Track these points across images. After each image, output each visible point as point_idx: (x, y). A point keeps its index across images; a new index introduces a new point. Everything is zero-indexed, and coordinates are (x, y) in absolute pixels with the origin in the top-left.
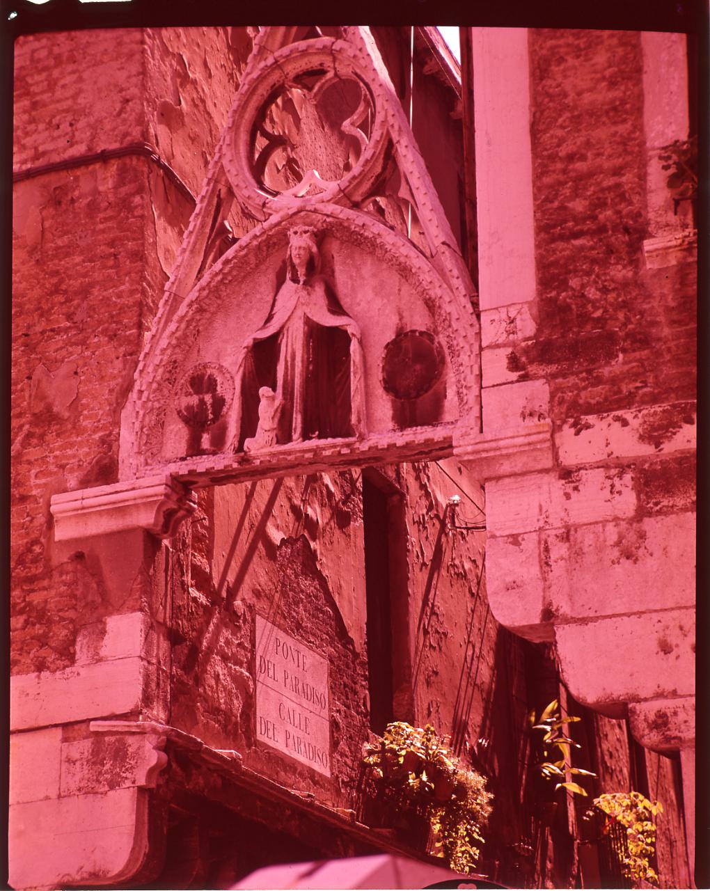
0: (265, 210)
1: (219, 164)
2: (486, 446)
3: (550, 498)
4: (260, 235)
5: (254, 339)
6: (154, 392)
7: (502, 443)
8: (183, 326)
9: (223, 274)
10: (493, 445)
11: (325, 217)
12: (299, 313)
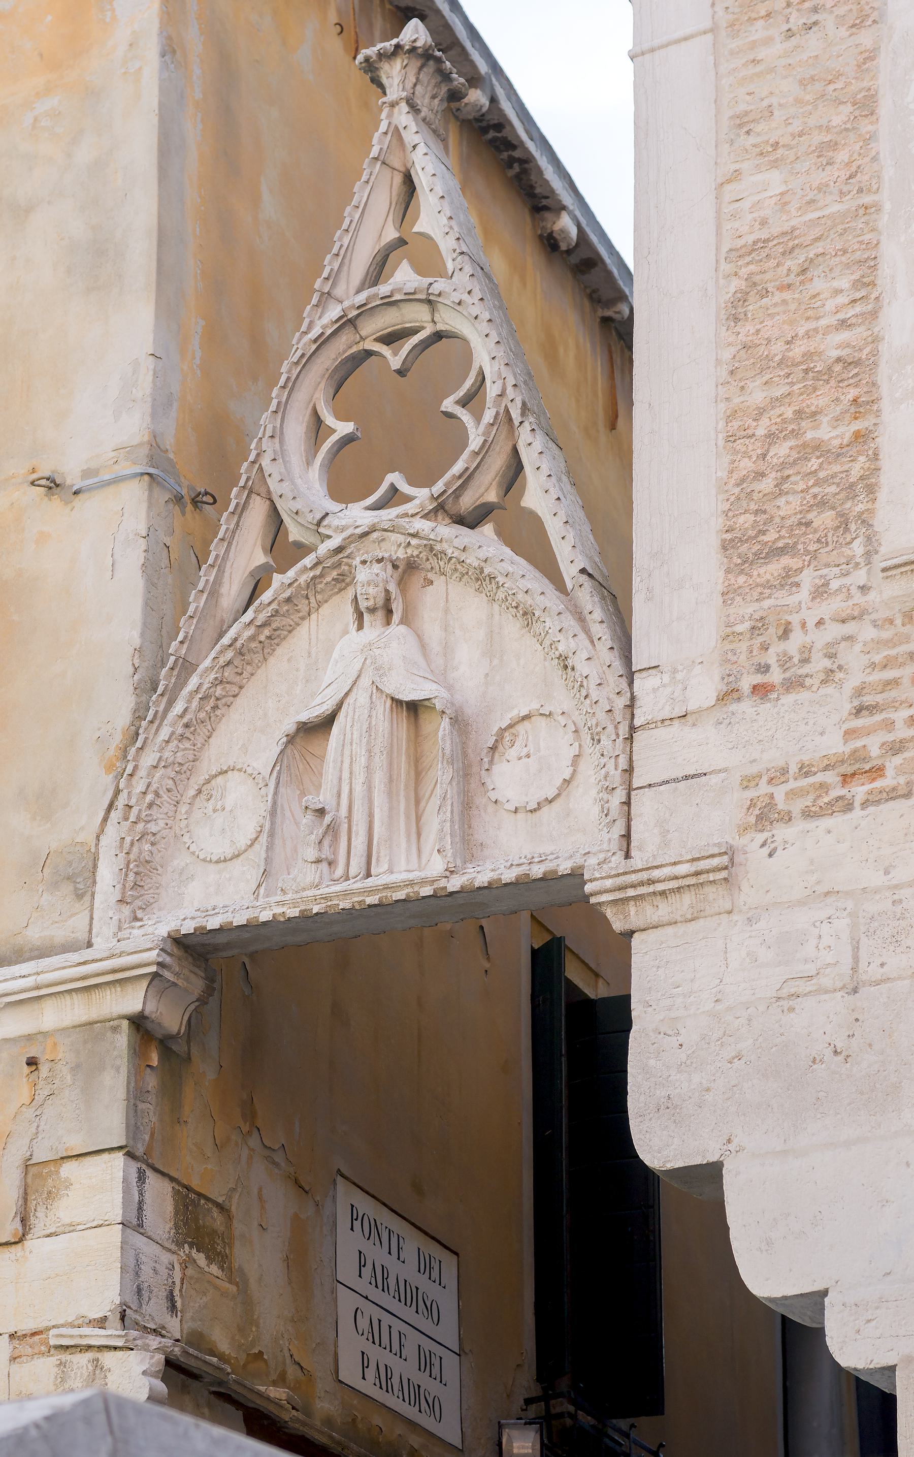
2: (633, 878)
4: (311, 569)
7: (656, 874)
10: (644, 876)
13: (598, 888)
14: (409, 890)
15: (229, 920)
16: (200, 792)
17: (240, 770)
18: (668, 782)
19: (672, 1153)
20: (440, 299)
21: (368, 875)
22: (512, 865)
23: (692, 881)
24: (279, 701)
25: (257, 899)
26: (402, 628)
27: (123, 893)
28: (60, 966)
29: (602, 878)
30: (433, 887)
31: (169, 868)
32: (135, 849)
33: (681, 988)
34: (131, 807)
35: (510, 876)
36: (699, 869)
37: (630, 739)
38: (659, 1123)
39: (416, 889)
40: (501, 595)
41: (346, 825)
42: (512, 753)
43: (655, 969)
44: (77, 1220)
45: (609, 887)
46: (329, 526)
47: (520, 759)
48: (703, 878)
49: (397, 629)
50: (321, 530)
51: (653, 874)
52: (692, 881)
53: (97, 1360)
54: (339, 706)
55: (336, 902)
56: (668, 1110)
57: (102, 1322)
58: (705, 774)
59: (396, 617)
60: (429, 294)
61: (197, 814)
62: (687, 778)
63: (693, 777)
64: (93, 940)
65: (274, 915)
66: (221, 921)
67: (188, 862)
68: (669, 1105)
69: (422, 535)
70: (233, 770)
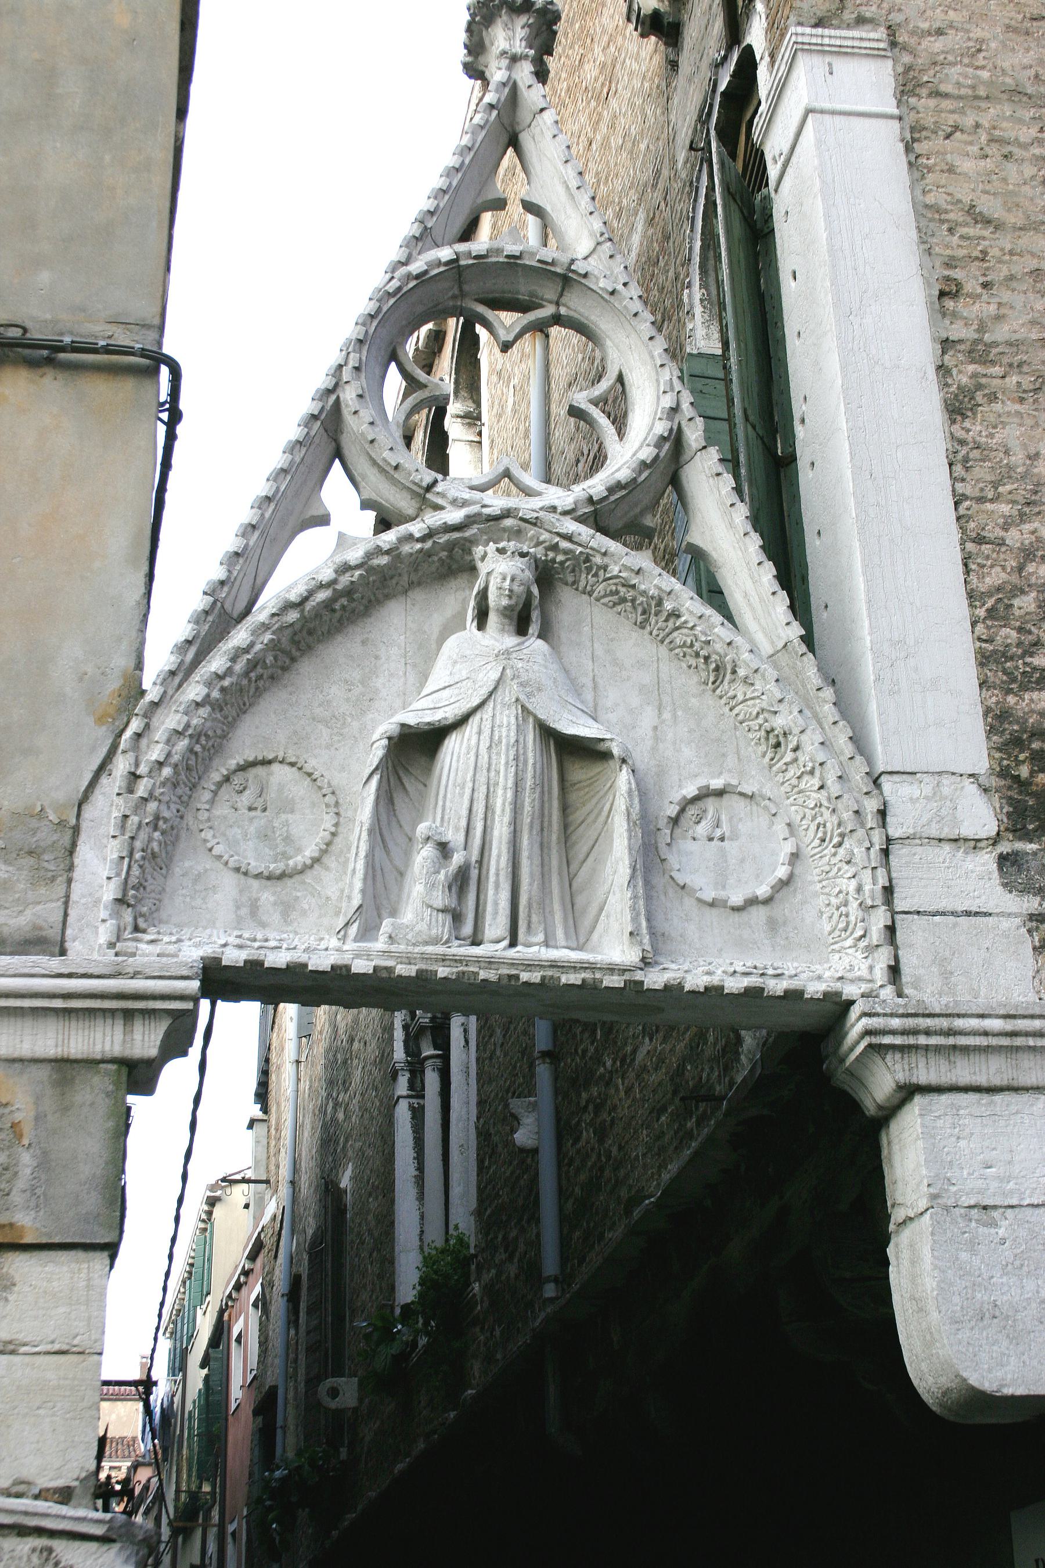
0: (428, 496)
1: (333, 398)
2: (929, 1022)
3: (895, 971)
4: (418, 540)
5: (403, 725)
6: (163, 784)
7: (960, 1023)
8: (239, 667)
9: (335, 590)
10: (944, 1023)
11: (557, 539)
12: (510, 692)
13: (882, 1027)
14: (587, 975)
15: (262, 958)
16: (227, 779)
17: (292, 764)
18: (943, 914)
19: (1009, 1376)
20: (583, 281)
21: (513, 944)
22: (735, 972)
23: (1005, 1041)
24: (350, 690)
25: (344, 939)
26: (540, 643)
27: (125, 894)
28: (26, 971)
29: (885, 1015)
30: (624, 978)
31: (178, 869)
32: (143, 836)
33: (993, 1170)
34: (140, 777)
35: (737, 985)
36: (1017, 1028)
37: (886, 852)
38: (985, 1334)
39: (598, 975)
40: (678, 637)
41: (477, 871)
42: (702, 829)
43: (954, 1139)
44: (21, 1337)
45: (895, 1027)
46: (442, 495)
47: (711, 839)
48: (1019, 1041)
49: (535, 645)
50: (428, 496)
51: (955, 1023)
52: (1005, 1041)
53: (50, 1550)
54: (462, 721)
55: (476, 970)
56: (995, 1321)
57: (65, 1495)
58: (990, 914)
59: (534, 629)
60: (569, 269)
61: (222, 810)
62: (968, 914)
63: (977, 914)
64: (67, 945)
65: (375, 968)
66: (288, 959)
67: (208, 867)
68: (997, 1314)
69: (575, 540)
70: (281, 762)
